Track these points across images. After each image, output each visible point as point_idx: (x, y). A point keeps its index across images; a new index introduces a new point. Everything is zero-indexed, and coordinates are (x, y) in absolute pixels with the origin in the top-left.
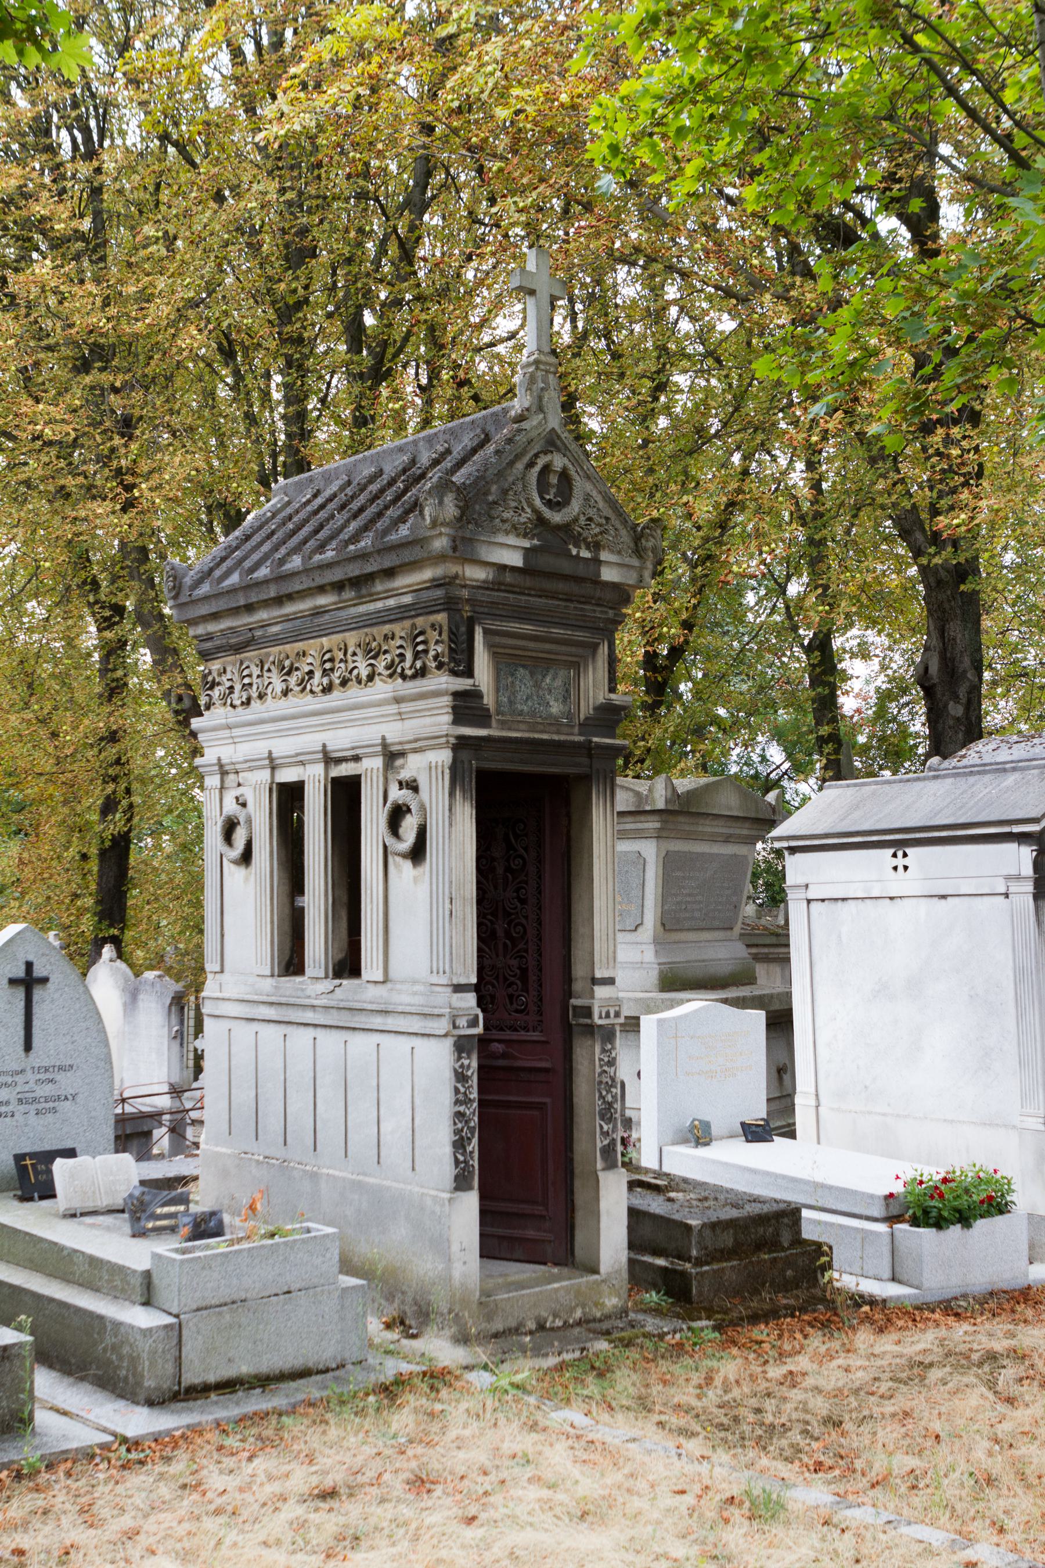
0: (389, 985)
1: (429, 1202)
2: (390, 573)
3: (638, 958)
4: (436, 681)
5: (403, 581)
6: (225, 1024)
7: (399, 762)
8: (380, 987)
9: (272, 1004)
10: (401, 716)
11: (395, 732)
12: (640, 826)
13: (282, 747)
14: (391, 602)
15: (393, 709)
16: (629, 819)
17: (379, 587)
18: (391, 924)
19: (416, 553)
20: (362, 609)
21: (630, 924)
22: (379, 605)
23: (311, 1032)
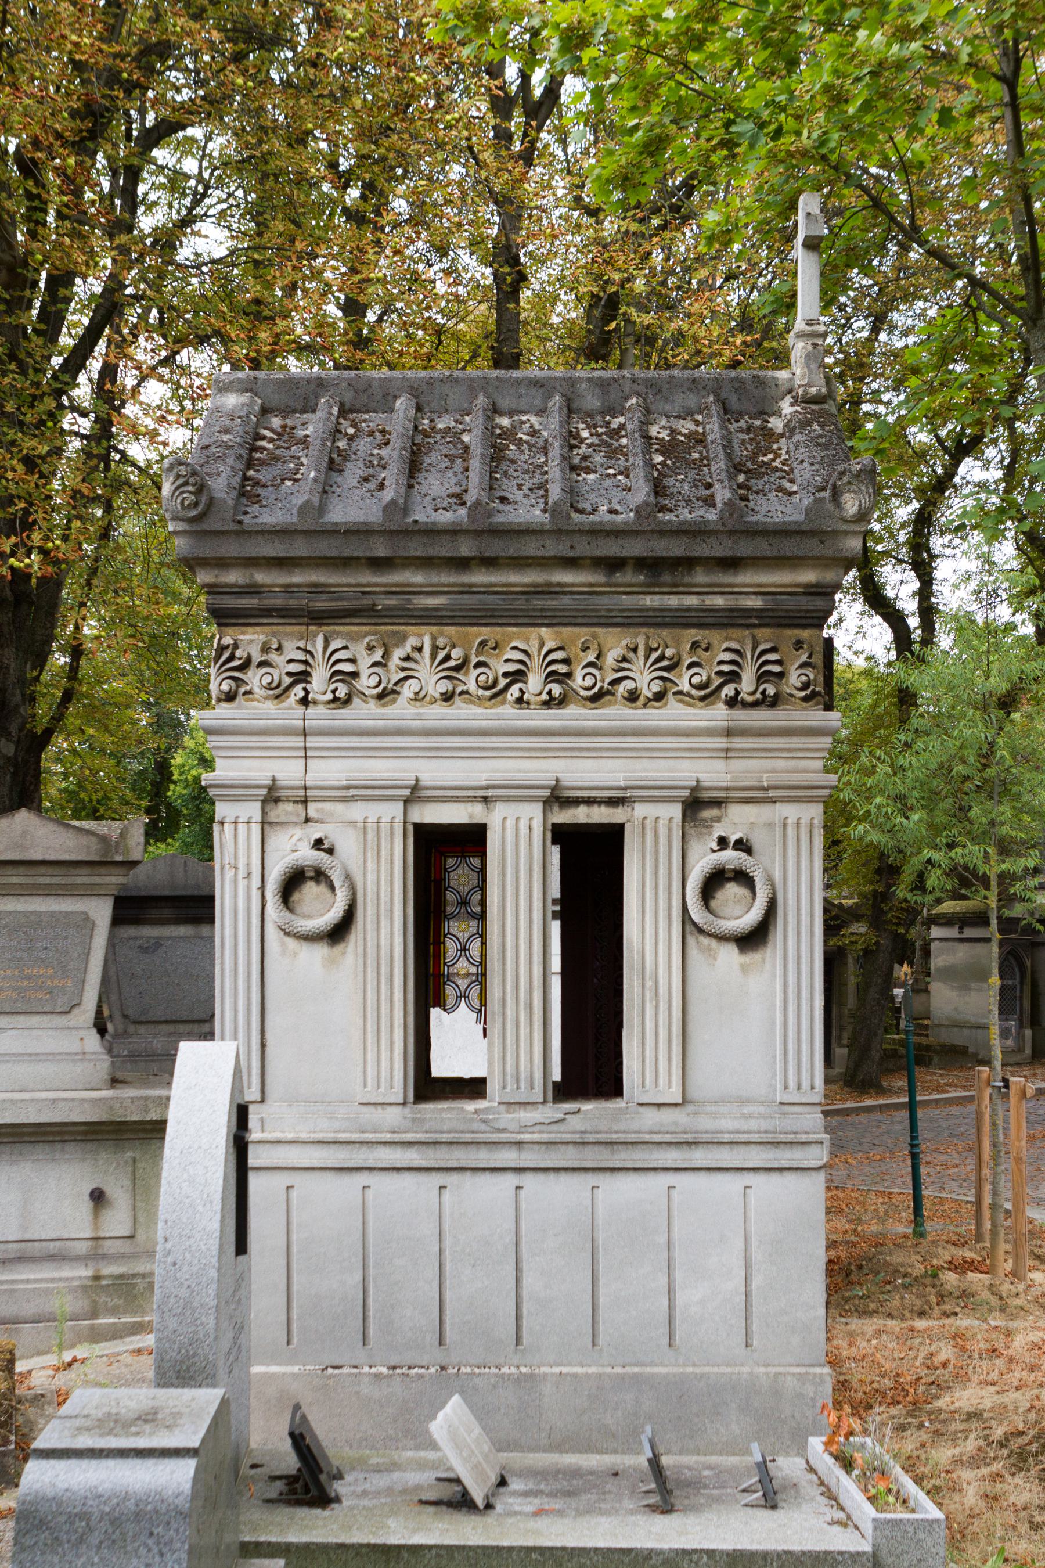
0: (690, 1108)
1: (791, 1383)
2: (731, 564)
3: (75, 1047)
4: (797, 714)
5: (746, 578)
6: (281, 1180)
7: (708, 813)
8: (677, 1110)
9: (410, 1144)
10: (727, 754)
11: (713, 774)
12: (97, 880)
13: (433, 772)
14: (719, 601)
15: (721, 742)
16: (85, 870)
17: (700, 577)
18: (690, 1027)
19: (811, 547)
20: (648, 601)
21: (61, 1004)
22: (692, 601)
23: (510, 1180)
